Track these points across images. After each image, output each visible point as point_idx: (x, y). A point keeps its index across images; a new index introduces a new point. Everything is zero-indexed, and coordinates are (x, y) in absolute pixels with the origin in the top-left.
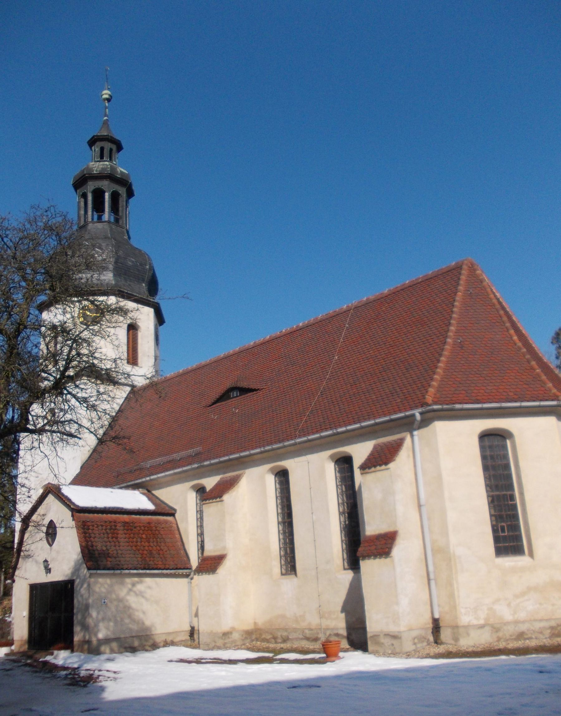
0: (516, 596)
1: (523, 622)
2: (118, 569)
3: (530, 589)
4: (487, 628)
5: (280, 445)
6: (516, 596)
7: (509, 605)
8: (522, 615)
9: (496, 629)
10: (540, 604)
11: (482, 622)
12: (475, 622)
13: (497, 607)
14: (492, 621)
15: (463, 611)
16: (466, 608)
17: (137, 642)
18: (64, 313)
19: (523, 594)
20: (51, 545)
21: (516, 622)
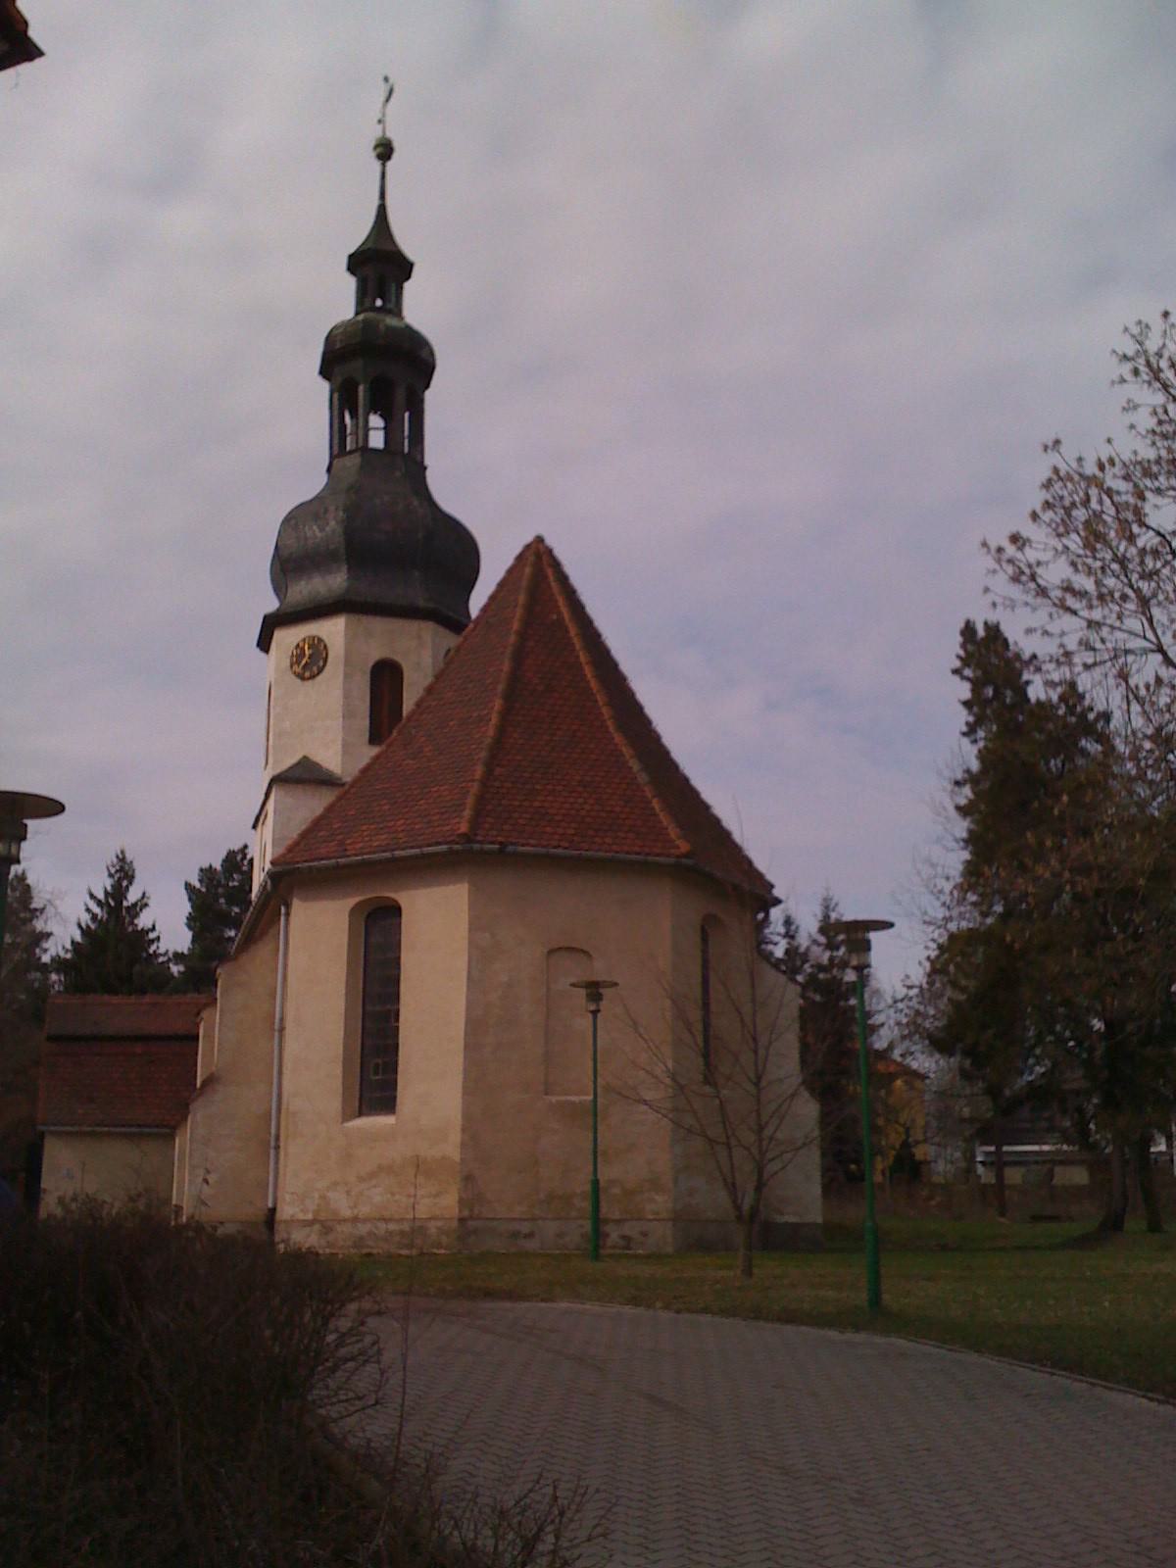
0: (361, 1179)
1: (365, 1220)
2: (506, 714)
3: (381, 1168)
4: (317, 1227)
5: (426, 850)
6: (361, 1179)
7: (348, 1193)
8: (364, 1210)
9: (327, 1229)
10: (393, 1194)
11: (310, 1216)
12: (301, 1216)
13: (331, 1195)
14: (323, 1216)
15: (288, 1197)
16: (292, 1193)
17: (392, 1429)
18: (301, 592)
19: (372, 1175)
20: (51, 808)
21: (355, 1220)
